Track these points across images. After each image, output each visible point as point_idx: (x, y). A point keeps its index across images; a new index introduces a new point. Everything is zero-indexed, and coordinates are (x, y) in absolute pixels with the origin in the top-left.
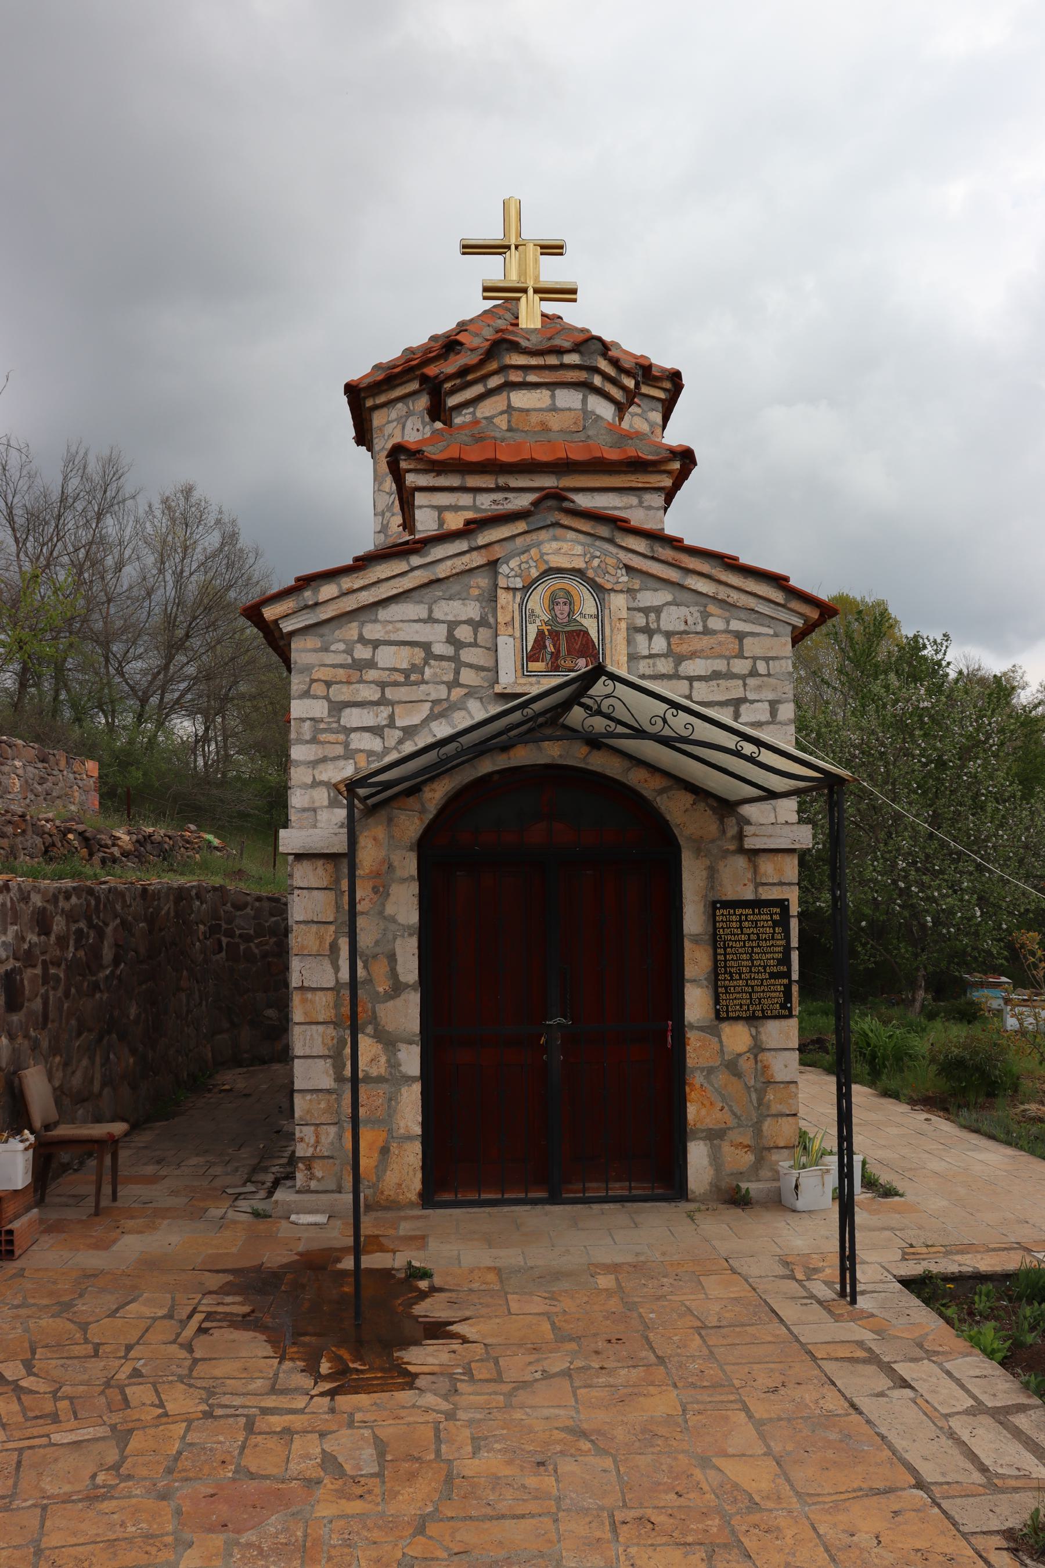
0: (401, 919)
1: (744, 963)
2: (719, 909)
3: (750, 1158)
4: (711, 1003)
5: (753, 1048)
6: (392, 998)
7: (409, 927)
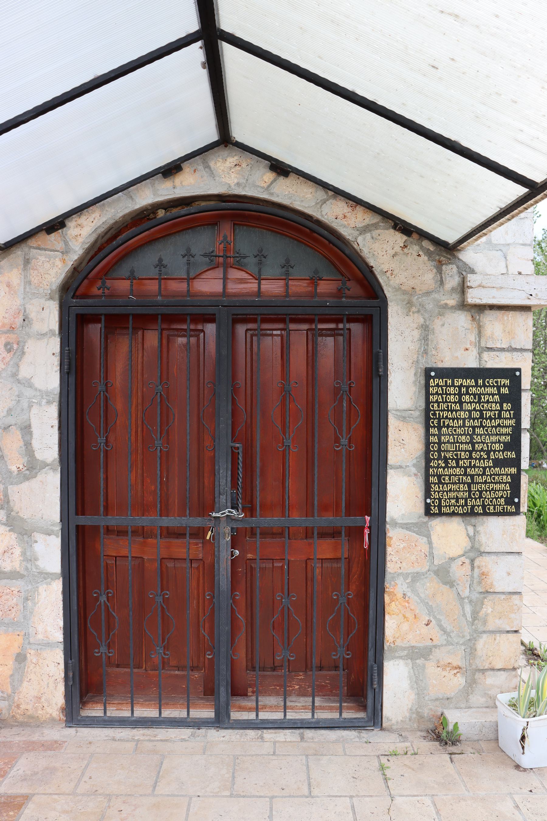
0: (38, 383)
1: (464, 447)
2: (433, 378)
3: (460, 681)
4: (421, 494)
5: (470, 551)
6: (27, 478)
7: (48, 393)
